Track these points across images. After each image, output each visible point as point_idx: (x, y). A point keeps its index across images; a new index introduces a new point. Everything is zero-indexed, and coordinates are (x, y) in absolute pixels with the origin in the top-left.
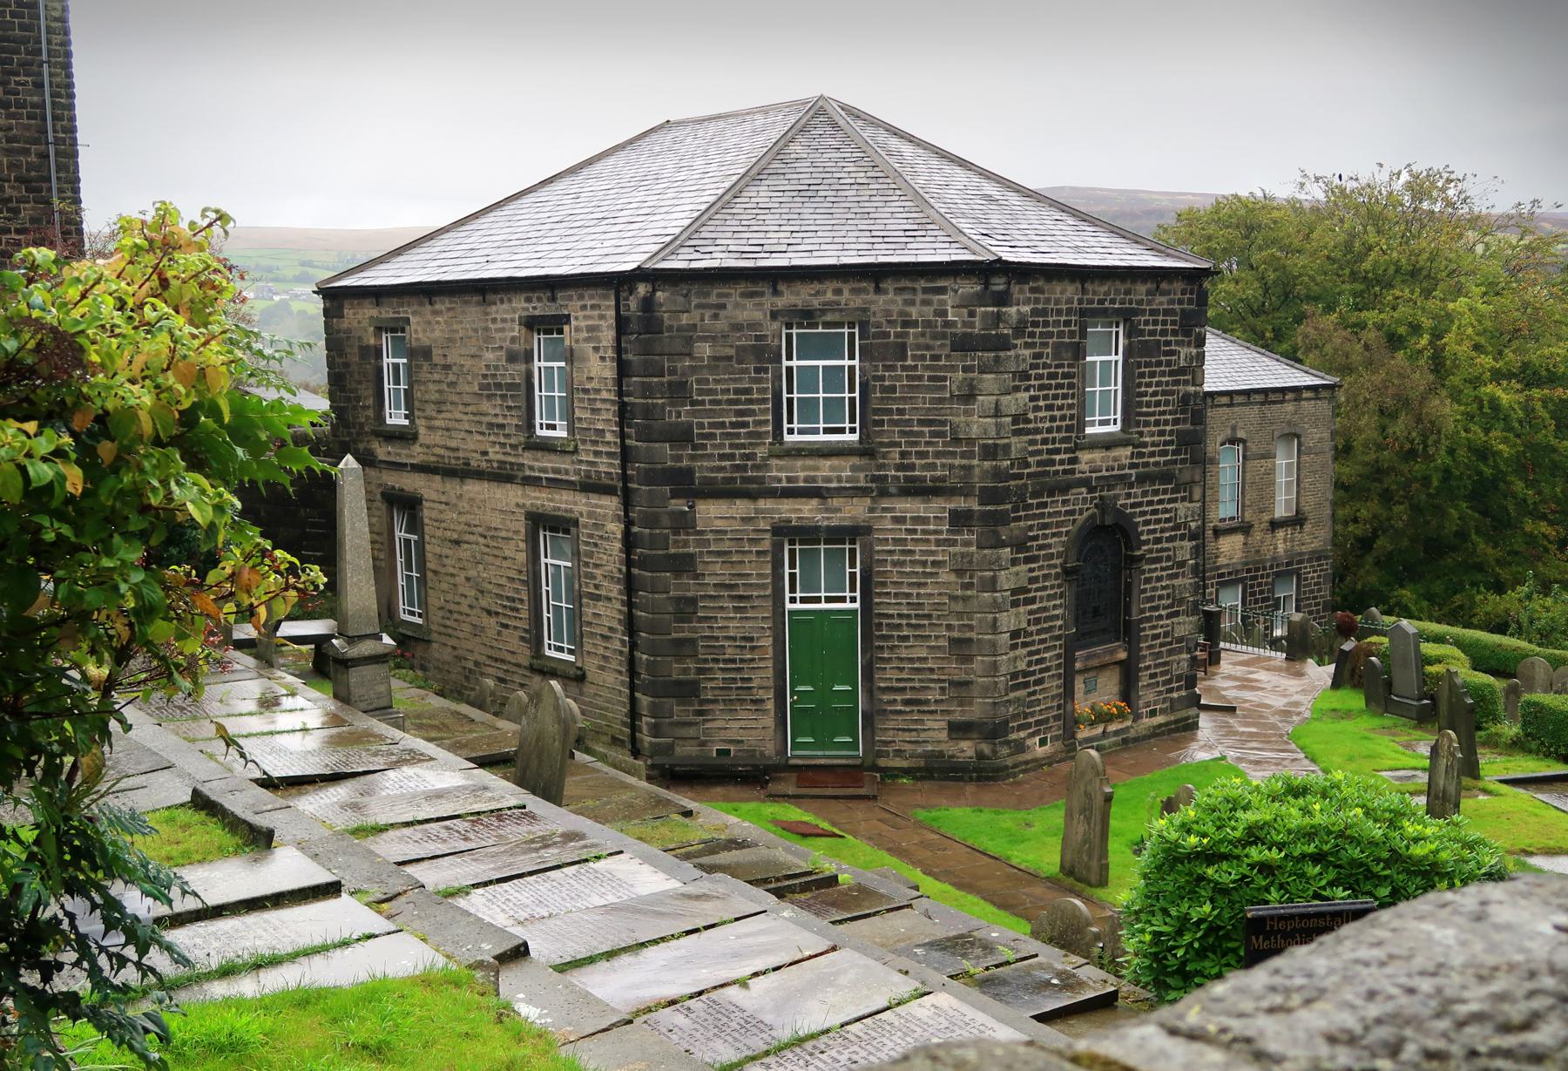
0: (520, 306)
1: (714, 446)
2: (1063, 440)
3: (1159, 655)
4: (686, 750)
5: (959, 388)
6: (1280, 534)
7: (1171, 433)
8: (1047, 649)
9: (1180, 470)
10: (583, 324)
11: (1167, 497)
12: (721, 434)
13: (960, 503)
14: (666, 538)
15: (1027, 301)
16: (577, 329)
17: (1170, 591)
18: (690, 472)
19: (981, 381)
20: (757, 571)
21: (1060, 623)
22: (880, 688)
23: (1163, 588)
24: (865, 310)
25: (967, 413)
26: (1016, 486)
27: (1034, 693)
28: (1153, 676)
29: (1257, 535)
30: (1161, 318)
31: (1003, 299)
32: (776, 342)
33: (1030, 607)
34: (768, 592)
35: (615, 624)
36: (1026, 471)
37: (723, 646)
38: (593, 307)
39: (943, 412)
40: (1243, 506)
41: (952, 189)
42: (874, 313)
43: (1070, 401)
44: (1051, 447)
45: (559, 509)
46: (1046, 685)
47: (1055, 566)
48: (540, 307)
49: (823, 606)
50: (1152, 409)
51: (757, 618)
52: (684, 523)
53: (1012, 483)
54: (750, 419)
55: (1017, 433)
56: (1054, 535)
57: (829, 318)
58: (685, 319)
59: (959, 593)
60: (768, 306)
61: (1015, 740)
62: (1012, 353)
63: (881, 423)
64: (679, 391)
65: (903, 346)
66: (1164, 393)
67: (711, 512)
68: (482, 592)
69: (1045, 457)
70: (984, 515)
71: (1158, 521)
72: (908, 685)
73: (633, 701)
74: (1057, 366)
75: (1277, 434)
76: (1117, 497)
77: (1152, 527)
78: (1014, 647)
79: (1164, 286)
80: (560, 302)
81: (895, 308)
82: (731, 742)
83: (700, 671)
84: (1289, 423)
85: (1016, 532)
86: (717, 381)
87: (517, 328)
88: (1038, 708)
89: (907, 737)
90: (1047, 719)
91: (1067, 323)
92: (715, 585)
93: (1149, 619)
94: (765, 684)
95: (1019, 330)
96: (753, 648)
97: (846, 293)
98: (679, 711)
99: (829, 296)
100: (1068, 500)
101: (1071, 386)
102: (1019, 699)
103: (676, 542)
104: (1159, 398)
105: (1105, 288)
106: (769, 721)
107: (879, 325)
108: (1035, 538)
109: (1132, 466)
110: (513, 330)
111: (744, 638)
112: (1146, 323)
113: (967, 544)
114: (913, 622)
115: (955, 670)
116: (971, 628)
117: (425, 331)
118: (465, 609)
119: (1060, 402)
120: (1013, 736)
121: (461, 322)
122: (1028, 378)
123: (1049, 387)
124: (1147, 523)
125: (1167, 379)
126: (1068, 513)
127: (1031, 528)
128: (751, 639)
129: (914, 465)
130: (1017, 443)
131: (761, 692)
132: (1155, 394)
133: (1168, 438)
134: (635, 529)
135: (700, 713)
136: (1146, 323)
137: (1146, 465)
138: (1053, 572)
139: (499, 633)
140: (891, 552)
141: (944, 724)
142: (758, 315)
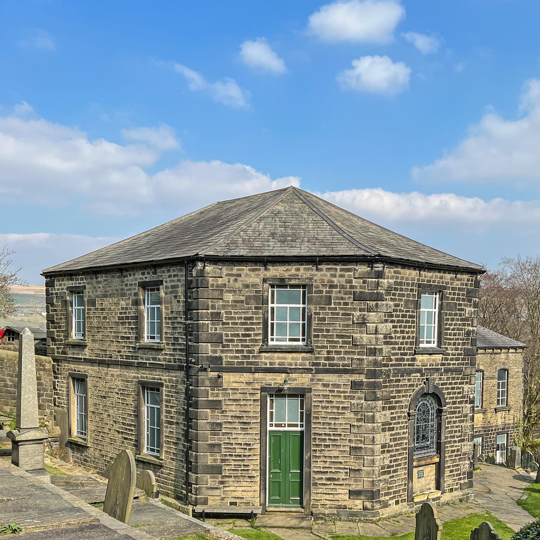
0: (139, 277)
2: (409, 349)
6: (499, 414)
7: (461, 349)
8: (400, 454)
9: (465, 368)
10: (169, 284)
11: (459, 381)
12: (237, 340)
13: (356, 377)
14: (207, 391)
15: (392, 278)
16: (167, 287)
17: (460, 428)
18: (220, 358)
21: (406, 441)
23: (457, 427)
24: (311, 279)
25: (361, 332)
27: (393, 477)
28: (451, 471)
30: (457, 292)
31: (380, 275)
32: (266, 294)
33: (391, 432)
34: (259, 421)
35: (180, 436)
36: (390, 363)
37: (235, 448)
38: (174, 276)
39: (349, 331)
40: (482, 401)
42: (316, 280)
43: (412, 330)
44: (402, 351)
45: (154, 379)
46: (399, 473)
47: (404, 413)
48: (149, 277)
49: (287, 429)
50: (452, 337)
52: (216, 383)
53: (383, 368)
54: (252, 333)
55: (386, 343)
56: (403, 396)
57: (293, 282)
58: (220, 281)
59: (356, 424)
60: (262, 276)
63: (317, 336)
67: (229, 379)
68: (115, 422)
69: (399, 356)
70: (369, 384)
72: (329, 470)
74: (406, 311)
76: (434, 379)
78: (383, 452)
79: (459, 276)
81: (326, 279)
82: (238, 498)
85: (385, 393)
87: (137, 288)
88: (395, 485)
89: (327, 497)
91: (412, 290)
92: (232, 416)
93: (450, 442)
94: (256, 468)
95: (389, 291)
96: (250, 449)
97: (302, 271)
99: (293, 272)
100: (411, 379)
101: (413, 322)
103: (212, 394)
104: (456, 331)
105: (430, 274)
108: (394, 397)
109: (443, 364)
110: (135, 289)
111: (246, 444)
112: (450, 294)
113: (360, 398)
114: (332, 438)
115: (353, 464)
117: (93, 292)
118: (106, 431)
119: (407, 330)
120: (382, 499)
121: (111, 287)
122: (392, 316)
123: (402, 322)
124: (449, 393)
125: (459, 322)
126: (410, 385)
128: (250, 444)
129: (334, 358)
130: (386, 349)
135: (222, 483)
136: (450, 294)
137: (449, 364)
138: (403, 415)
139: (123, 442)
141: (347, 491)
142: (258, 281)
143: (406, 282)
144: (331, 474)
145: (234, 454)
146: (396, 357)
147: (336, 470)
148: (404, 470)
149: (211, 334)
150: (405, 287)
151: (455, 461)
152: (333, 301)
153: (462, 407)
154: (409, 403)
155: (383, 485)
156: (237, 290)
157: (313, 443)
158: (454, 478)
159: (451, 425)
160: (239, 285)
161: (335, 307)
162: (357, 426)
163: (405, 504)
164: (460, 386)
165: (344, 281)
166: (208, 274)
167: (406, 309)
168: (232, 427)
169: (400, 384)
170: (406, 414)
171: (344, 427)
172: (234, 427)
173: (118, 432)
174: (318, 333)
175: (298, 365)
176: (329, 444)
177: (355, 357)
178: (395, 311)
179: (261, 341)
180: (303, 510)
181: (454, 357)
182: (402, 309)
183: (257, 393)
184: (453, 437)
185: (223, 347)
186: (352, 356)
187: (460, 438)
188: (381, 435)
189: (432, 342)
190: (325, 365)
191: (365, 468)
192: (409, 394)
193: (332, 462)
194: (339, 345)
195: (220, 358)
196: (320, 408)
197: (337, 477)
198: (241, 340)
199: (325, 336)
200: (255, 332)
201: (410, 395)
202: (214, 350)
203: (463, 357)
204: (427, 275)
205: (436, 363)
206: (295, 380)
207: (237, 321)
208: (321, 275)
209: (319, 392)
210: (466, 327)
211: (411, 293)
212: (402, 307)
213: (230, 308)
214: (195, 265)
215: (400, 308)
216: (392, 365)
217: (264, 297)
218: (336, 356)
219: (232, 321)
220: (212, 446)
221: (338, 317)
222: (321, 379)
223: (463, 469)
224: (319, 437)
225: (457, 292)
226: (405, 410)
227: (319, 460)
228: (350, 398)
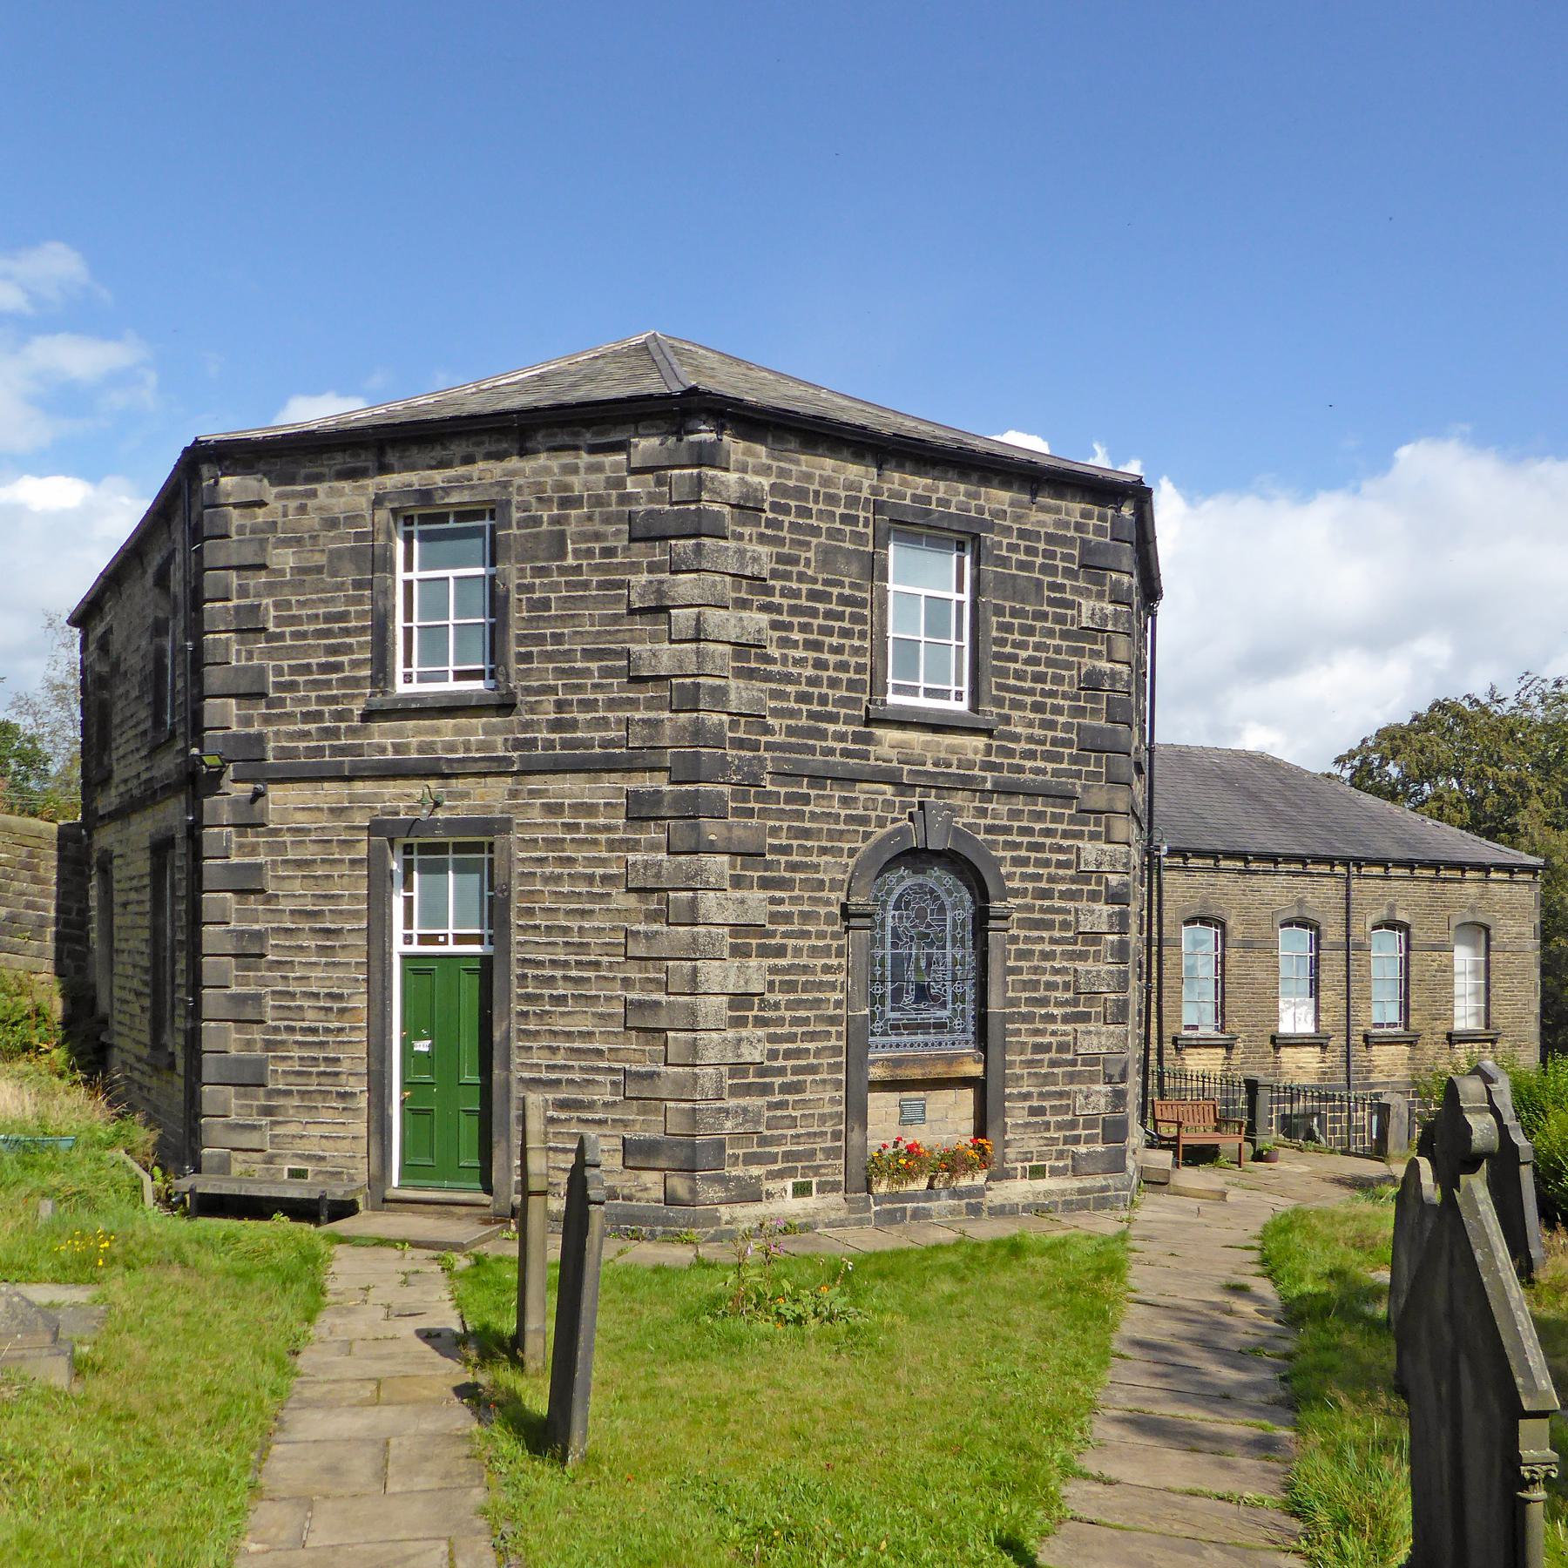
3: (1047, 1079)
7: (1067, 727)
8: (812, 1036)
11: (1060, 827)
12: (306, 682)
15: (765, 470)
18: (260, 739)
19: (675, 584)
20: (352, 888)
23: (1056, 971)
24: (505, 485)
25: (655, 638)
28: (1034, 1111)
30: (1042, 546)
31: (707, 457)
33: (772, 961)
36: (763, 739)
37: (300, 1008)
39: (620, 636)
41: (712, 360)
43: (857, 643)
44: (816, 708)
46: (807, 1096)
47: (828, 903)
49: (451, 948)
50: (1028, 685)
51: (348, 964)
54: (345, 659)
55: (750, 674)
56: (824, 851)
59: (642, 927)
60: (372, 490)
61: (738, 1178)
62: (731, 544)
64: (249, 627)
65: (562, 536)
66: (1050, 663)
70: (679, 799)
72: (564, 1076)
75: (1455, 922)
77: (1030, 870)
78: (740, 1022)
82: (309, 1158)
83: (269, 1045)
84: (1473, 909)
85: (738, 833)
86: (301, 604)
90: (812, 1153)
91: (847, 519)
93: (1026, 1018)
95: (748, 508)
101: (859, 619)
102: (745, 1110)
103: (241, 846)
108: (786, 850)
111: (330, 995)
112: (1013, 548)
113: (653, 847)
114: (573, 973)
115: (637, 1055)
120: (737, 1171)
122: (769, 591)
123: (814, 613)
124: (1017, 861)
125: (1057, 642)
126: (850, 819)
127: (775, 832)
128: (339, 997)
129: (575, 721)
130: (740, 693)
132: (1030, 661)
135: (267, 1111)
136: (1013, 548)
140: (541, 861)
141: (617, 1143)
143: (822, 490)
144: (570, 1089)
146: (792, 722)
147: (585, 1076)
148: (828, 1088)
150: (821, 506)
151: (1050, 1079)
152: (570, 547)
153: (1077, 910)
154: (848, 875)
155: (737, 1126)
156: (306, 536)
157: (520, 991)
158: (1047, 1135)
159: (1032, 964)
160: (312, 520)
161: (575, 563)
163: (836, 1198)
164: (1066, 843)
165: (602, 484)
166: (228, 495)
167: (825, 576)
168: (293, 943)
169: (807, 809)
170: (837, 910)
171: (607, 940)
172: (299, 943)
174: (529, 649)
175: (474, 748)
176: (564, 992)
177: (637, 716)
178: (775, 574)
179: (368, 682)
180: (486, 1199)
181: (1039, 748)
182: (810, 572)
183: (358, 841)
185: (268, 707)
186: (628, 714)
187: (1069, 1010)
188: (727, 964)
189: (953, 695)
190: (550, 744)
191: (671, 1070)
192: (846, 846)
193: (571, 1050)
194: (589, 682)
195: (260, 739)
196: (538, 880)
197: (589, 1097)
198: (316, 684)
199: (549, 657)
200: (354, 657)
201: (852, 852)
202: (245, 716)
203: (1075, 751)
204: (907, 486)
205: (959, 760)
206: (465, 795)
207: (305, 628)
208: (535, 472)
209: (536, 830)
210: (1086, 660)
213: (286, 590)
215: (801, 568)
216: (769, 747)
217: (377, 552)
218: (581, 716)
219: (293, 629)
221: (587, 593)
222: (539, 790)
223: (1082, 1108)
224: (536, 972)
225: (1042, 546)
227: (535, 1045)
228: (624, 847)
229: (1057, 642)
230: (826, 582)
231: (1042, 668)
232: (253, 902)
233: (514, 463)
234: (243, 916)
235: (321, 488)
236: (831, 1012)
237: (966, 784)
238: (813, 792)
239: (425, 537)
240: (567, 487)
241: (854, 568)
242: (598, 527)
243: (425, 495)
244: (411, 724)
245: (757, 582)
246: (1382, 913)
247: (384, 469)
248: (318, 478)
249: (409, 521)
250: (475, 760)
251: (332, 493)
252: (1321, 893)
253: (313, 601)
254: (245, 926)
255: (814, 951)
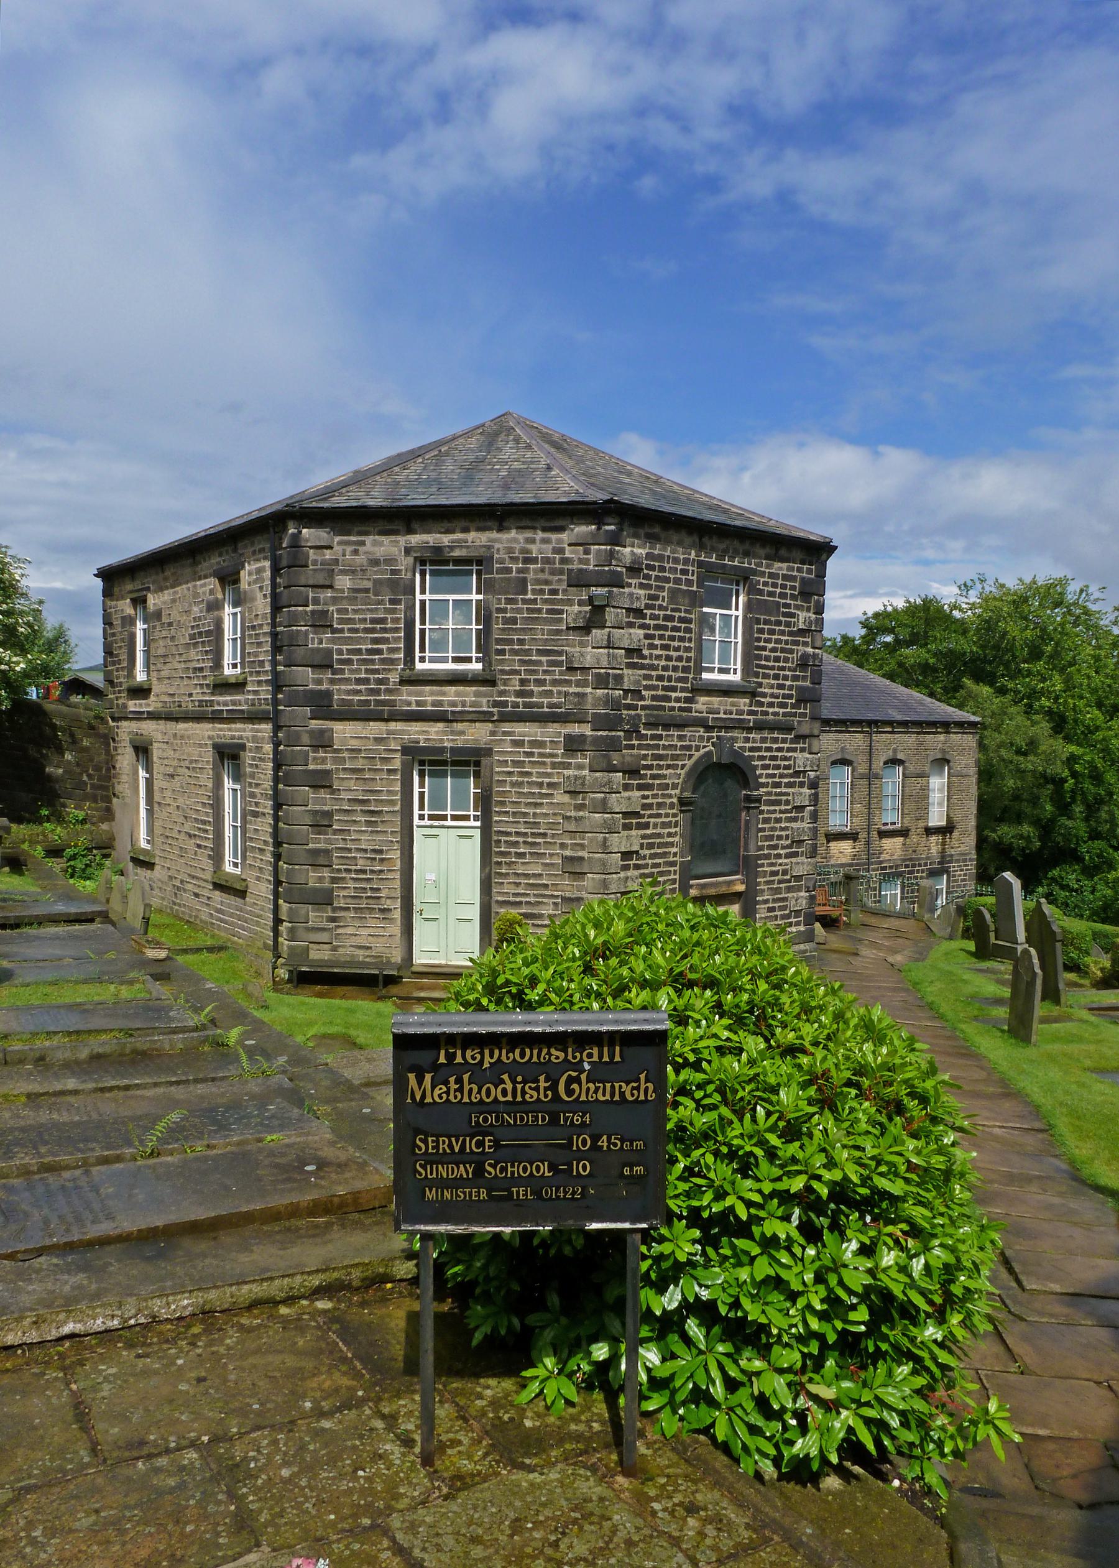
1: (352, 671)
2: (679, 679)
3: (778, 891)
4: (319, 954)
5: (575, 620)
7: (791, 688)
9: (799, 722)
11: (786, 746)
12: (358, 660)
13: (575, 729)
14: (307, 753)
17: (789, 832)
18: (328, 694)
21: (674, 850)
22: (497, 902)
23: (782, 829)
24: (489, 547)
26: (629, 715)
28: (771, 909)
29: (914, 838)
30: (780, 582)
34: (398, 808)
36: (640, 703)
37: (355, 858)
39: (560, 643)
42: (498, 550)
43: (687, 645)
44: (666, 684)
47: (671, 796)
52: (322, 742)
56: (669, 767)
57: (456, 553)
59: (573, 814)
62: (626, 590)
63: (502, 652)
64: (321, 622)
65: (525, 580)
66: (783, 650)
67: (344, 732)
69: (660, 693)
70: (596, 739)
71: (777, 767)
73: (276, 909)
75: (931, 758)
77: (770, 772)
78: (626, 868)
80: (240, 552)
83: (334, 880)
85: (628, 759)
86: (355, 611)
91: (684, 572)
93: (767, 857)
94: (393, 895)
95: (634, 569)
96: (382, 860)
98: (315, 917)
100: (685, 736)
103: (315, 758)
106: (396, 929)
107: (501, 561)
108: (650, 767)
109: (751, 713)
111: (375, 851)
112: (765, 584)
113: (580, 767)
114: (530, 840)
115: (568, 887)
116: (582, 847)
119: (676, 644)
122: (644, 617)
123: (665, 628)
124: (766, 767)
125: (786, 638)
126: (683, 748)
127: (645, 757)
128: (381, 852)
130: (630, 677)
131: (388, 901)
132: (774, 650)
133: (787, 692)
134: (282, 748)
135: (333, 920)
136: (765, 584)
140: (510, 773)
142: (394, 550)
145: (354, 868)
146: (654, 693)
149: (312, 649)
160: (361, 559)
162: (575, 818)
166: (307, 540)
169: (661, 743)
170: (675, 800)
173: (190, 836)
177: (572, 690)
178: (647, 607)
181: (776, 700)
182: (665, 604)
184: (775, 847)
190: (516, 705)
192: (680, 763)
199: (514, 652)
201: (683, 766)
208: (509, 540)
210: (800, 648)
211: (684, 577)
212: (663, 600)
213: (344, 602)
214: (285, 529)
215: (660, 602)
216: (644, 708)
218: (536, 689)
220: (316, 852)
225: (780, 582)
226: (673, 792)
229: (786, 638)
230: (673, 610)
231: (778, 654)
232: (323, 794)
233: (494, 535)
234: (316, 801)
235: (369, 539)
236: (672, 859)
237: (741, 726)
238: (664, 733)
239: (433, 573)
240: (529, 551)
241: (687, 601)
242: (546, 576)
243: (438, 550)
244: (428, 688)
245: (639, 613)
246: (889, 754)
247: (410, 531)
248: (367, 533)
249: (423, 562)
250: (468, 712)
251: (375, 543)
252: (854, 742)
253: (363, 610)
254: (317, 807)
255: (664, 825)
